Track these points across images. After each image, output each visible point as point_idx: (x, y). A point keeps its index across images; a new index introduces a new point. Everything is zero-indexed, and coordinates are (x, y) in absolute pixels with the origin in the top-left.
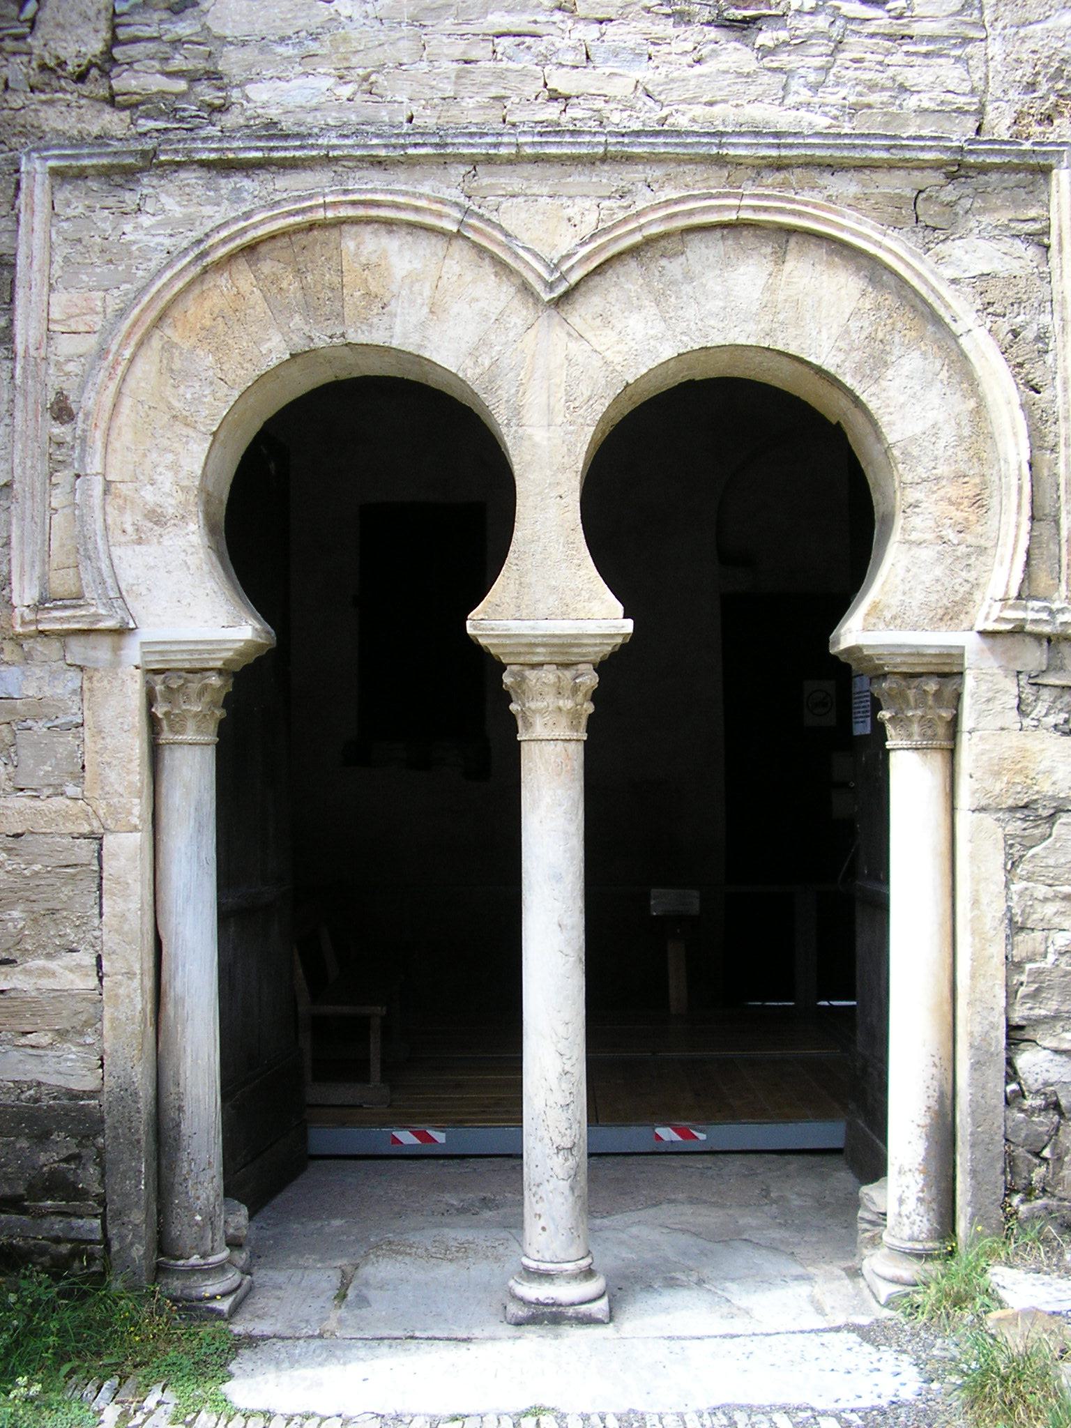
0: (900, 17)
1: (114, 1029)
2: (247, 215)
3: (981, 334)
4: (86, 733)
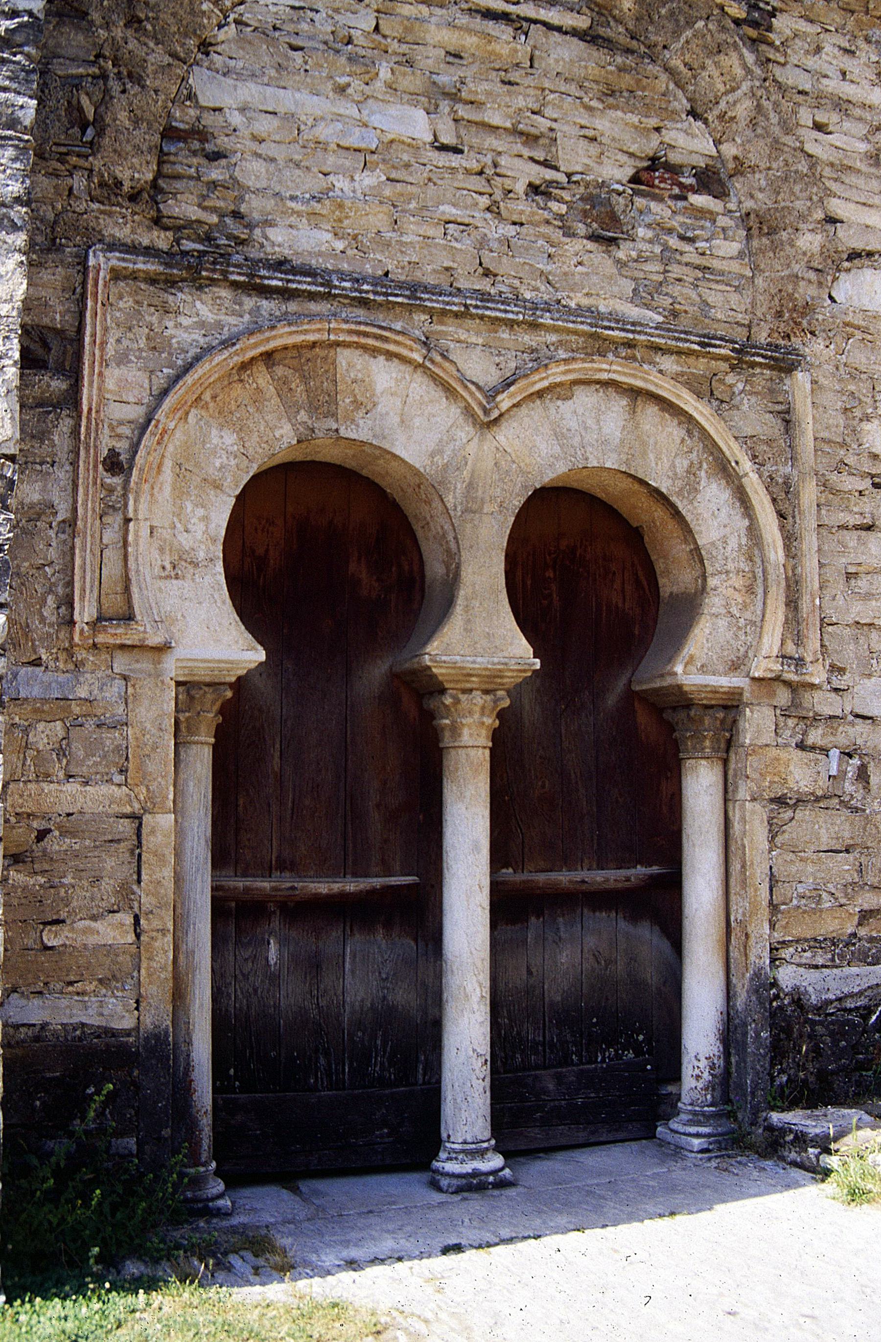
0: (703, 254)
1: (149, 975)
3: (754, 476)
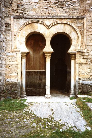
3: (78, 31)
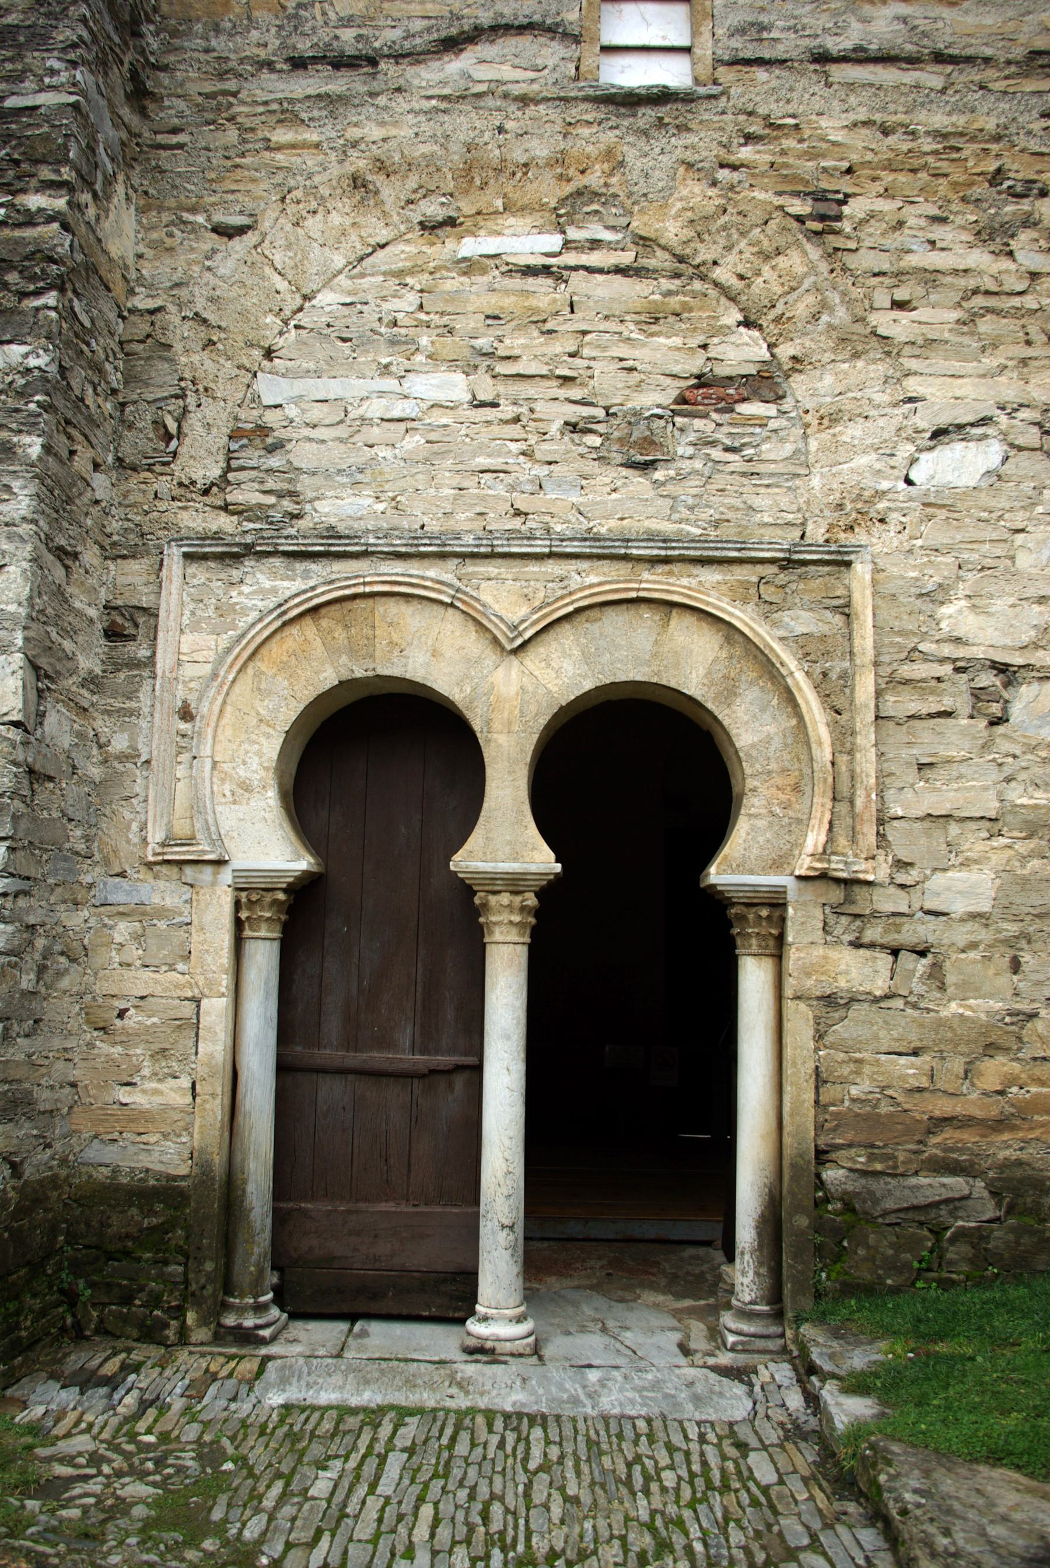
2: (313, 588)
4: (193, 929)
